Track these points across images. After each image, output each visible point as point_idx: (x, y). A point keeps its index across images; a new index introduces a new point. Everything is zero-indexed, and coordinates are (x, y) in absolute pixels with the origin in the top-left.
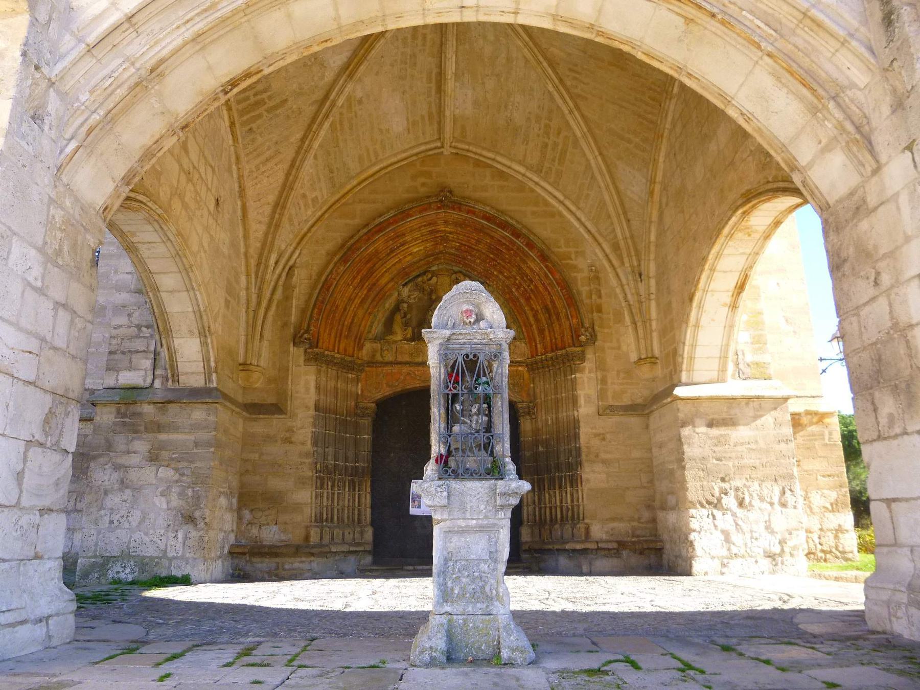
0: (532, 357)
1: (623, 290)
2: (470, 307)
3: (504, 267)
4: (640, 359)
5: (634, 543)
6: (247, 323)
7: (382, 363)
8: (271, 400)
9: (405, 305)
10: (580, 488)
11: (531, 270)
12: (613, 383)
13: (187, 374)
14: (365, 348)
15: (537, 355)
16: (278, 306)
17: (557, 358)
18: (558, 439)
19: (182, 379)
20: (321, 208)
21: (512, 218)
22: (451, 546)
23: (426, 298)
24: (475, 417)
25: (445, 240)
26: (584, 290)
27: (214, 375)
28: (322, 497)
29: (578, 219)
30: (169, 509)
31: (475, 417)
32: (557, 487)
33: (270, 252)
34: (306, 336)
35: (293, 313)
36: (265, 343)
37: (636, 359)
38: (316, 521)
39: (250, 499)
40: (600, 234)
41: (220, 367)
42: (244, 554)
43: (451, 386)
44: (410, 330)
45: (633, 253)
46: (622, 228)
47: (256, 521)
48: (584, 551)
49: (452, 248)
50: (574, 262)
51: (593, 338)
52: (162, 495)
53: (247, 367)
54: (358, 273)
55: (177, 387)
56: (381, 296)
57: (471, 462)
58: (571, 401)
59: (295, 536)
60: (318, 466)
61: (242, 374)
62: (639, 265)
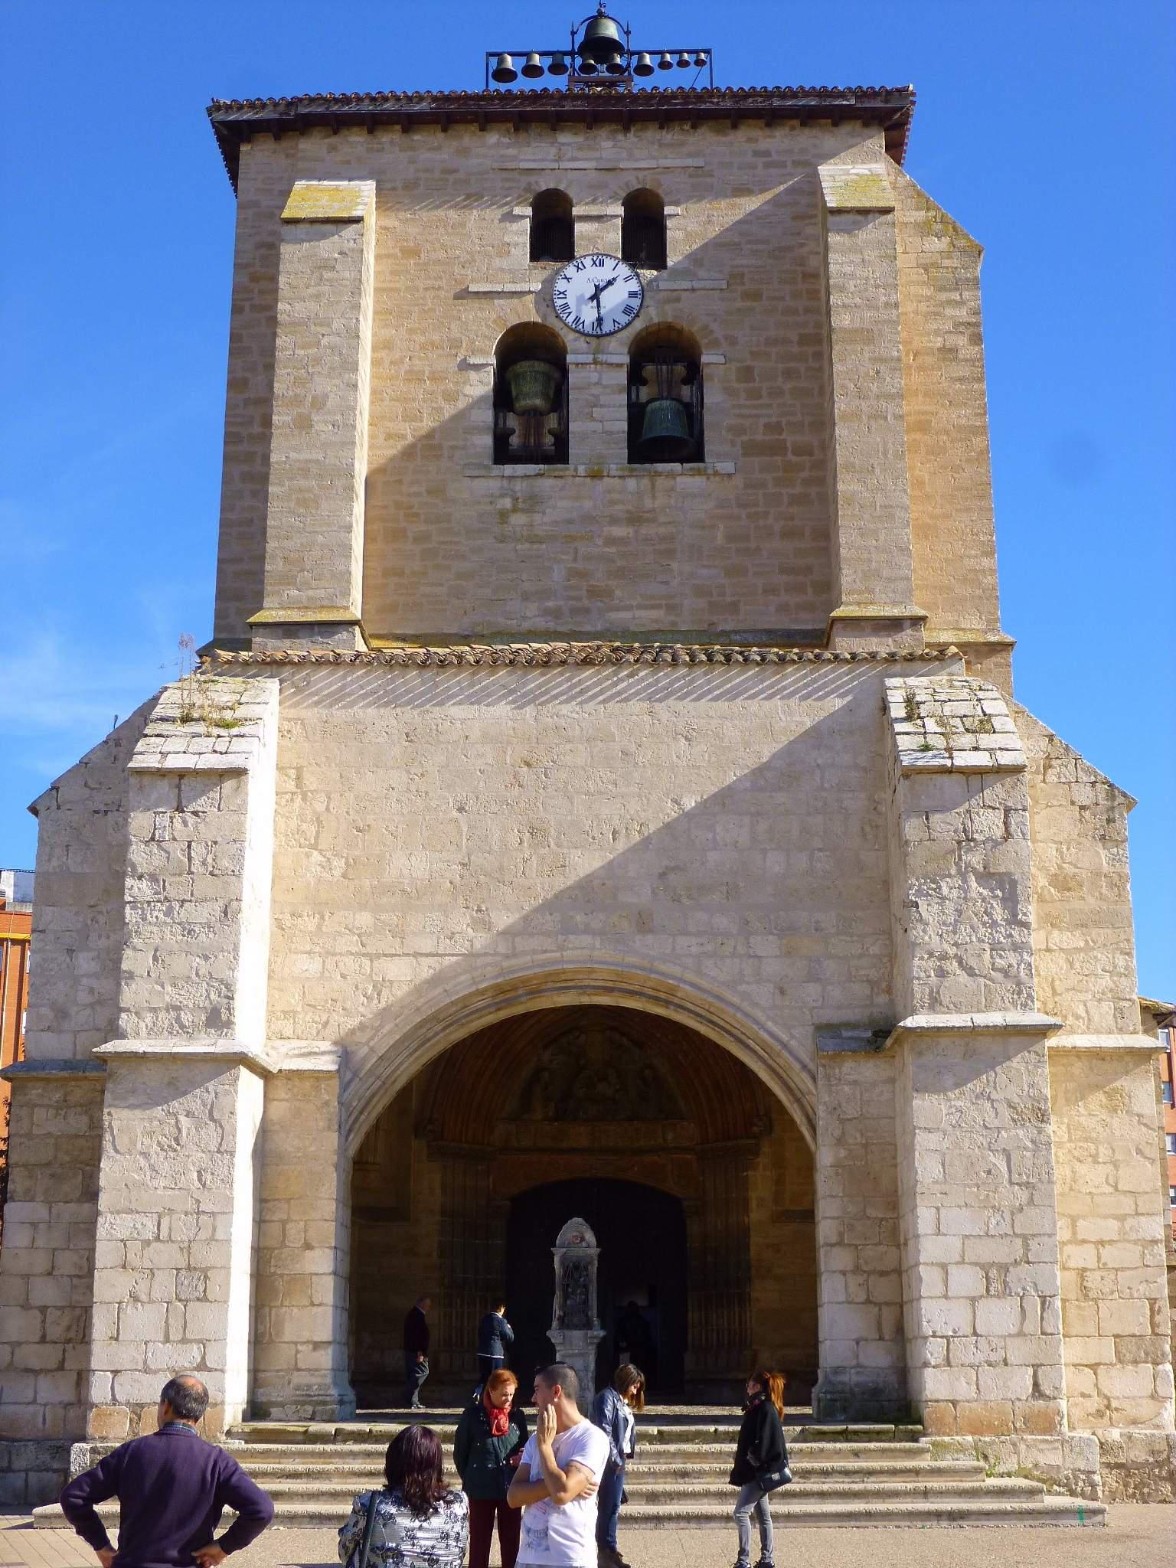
9: (546, 1074)
34: (430, 1127)
57: (575, 1320)
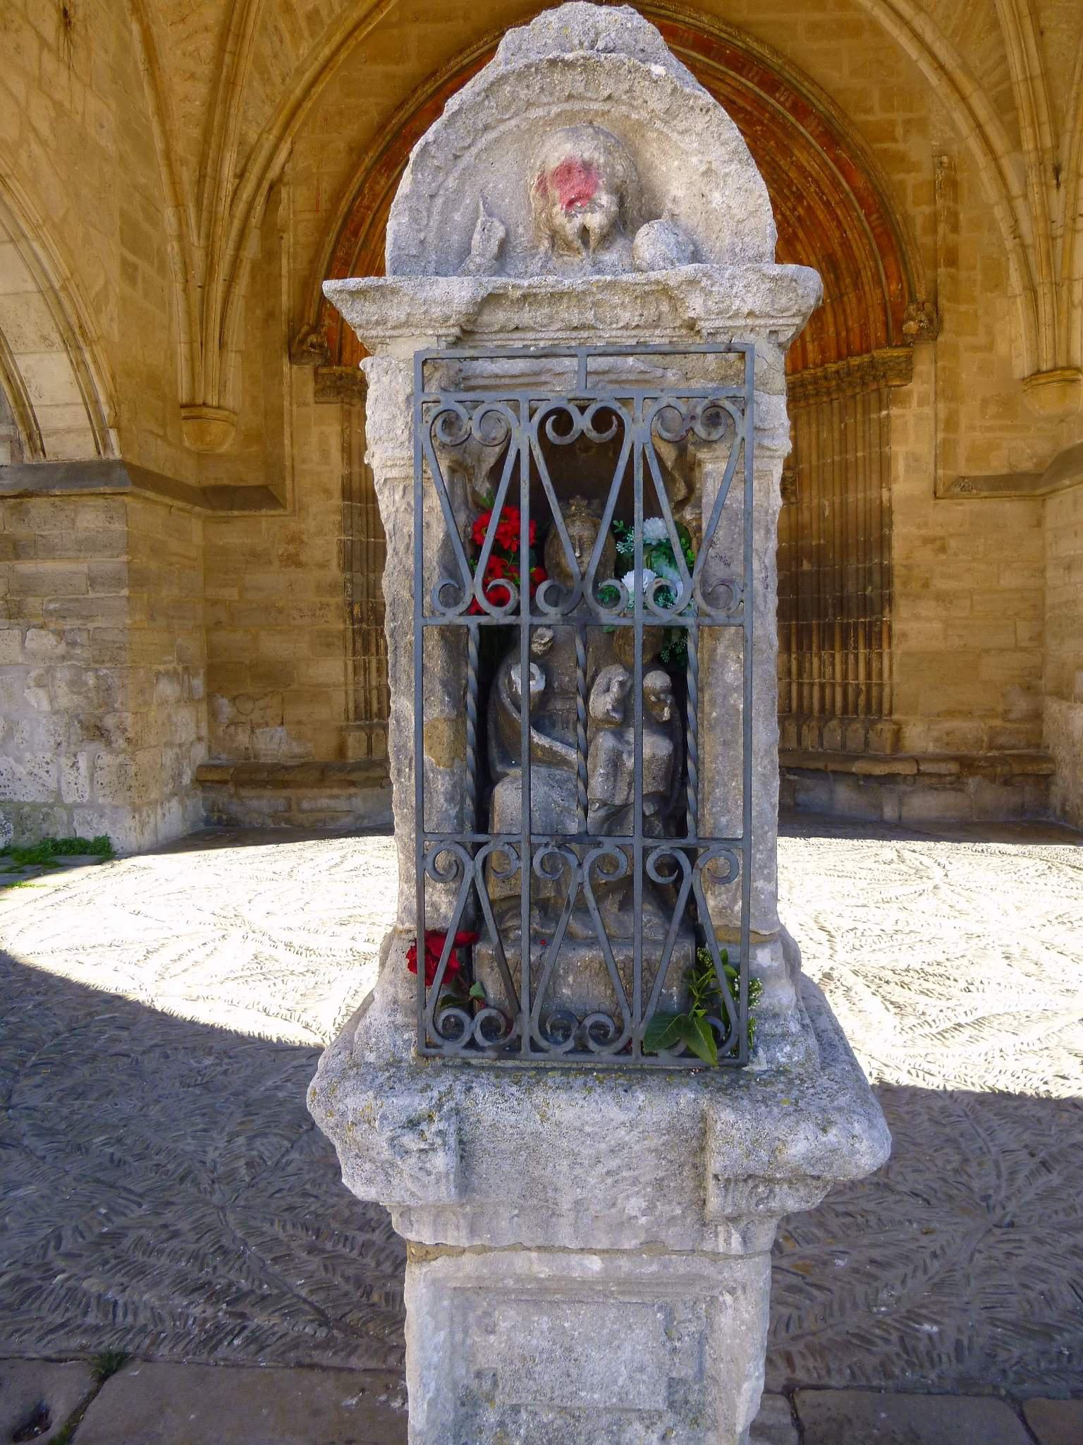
1: (1012, 210)
2: (585, 149)
4: (1039, 372)
5: (992, 762)
6: (188, 313)
8: (254, 478)
10: (886, 651)
11: (801, 169)
12: (972, 428)
13: (56, 432)
15: (806, 367)
16: (253, 277)
17: (849, 374)
18: (844, 546)
19: (49, 443)
20: (329, 39)
21: (759, 40)
22: (492, 1350)
24: (605, 742)
26: (919, 213)
27: (113, 434)
28: (366, 669)
29: (917, 37)
30: (56, 712)
31: (605, 742)
32: (837, 645)
33: (221, 149)
34: (313, 338)
35: (284, 288)
36: (233, 359)
37: (1027, 374)
38: (358, 718)
39: (228, 677)
40: (969, 73)
41: (125, 416)
42: (225, 782)
43: (474, 588)
45: (1044, 116)
46: (1024, 52)
47: (243, 718)
48: (891, 778)
50: (901, 146)
51: (934, 327)
52: (39, 686)
53: (195, 412)
55: (43, 461)
58: (876, 467)
59: (320, 748)
60: (357, 610)
61: (188, 427)
62: (1057, 147)
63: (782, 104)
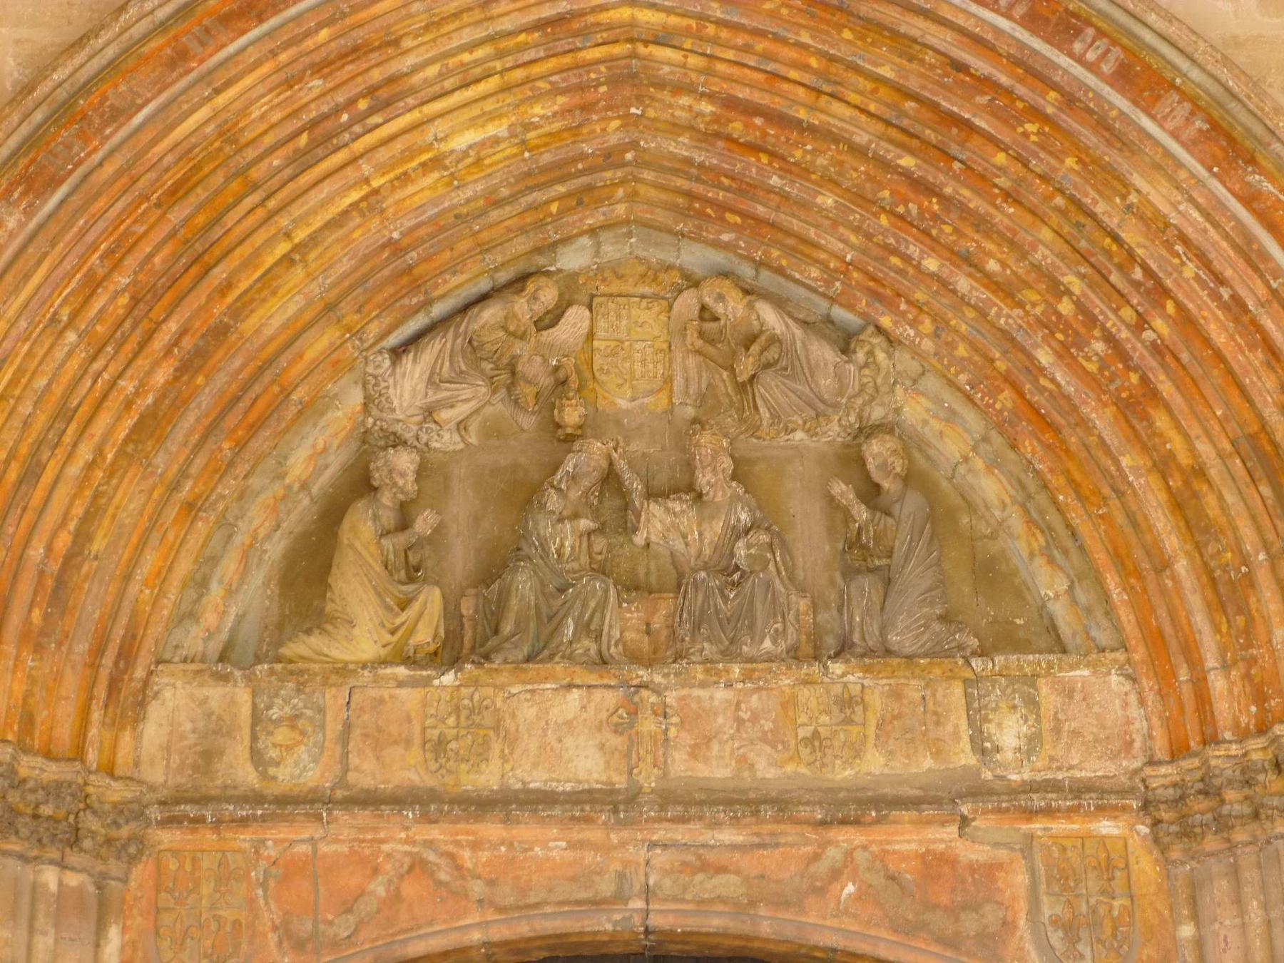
0: (1178, 751)
3: (982, 224)
7: (257, 799)
9: (405, 461)
14: (155, 712)
15: (1211, 739)
23: (528, 422)
25: (631, 80)
44: (431, 600)
49: (675, 128)
54: (114, 257)
56: (257, 411)
63: (1092, 68)
